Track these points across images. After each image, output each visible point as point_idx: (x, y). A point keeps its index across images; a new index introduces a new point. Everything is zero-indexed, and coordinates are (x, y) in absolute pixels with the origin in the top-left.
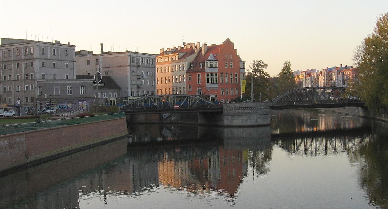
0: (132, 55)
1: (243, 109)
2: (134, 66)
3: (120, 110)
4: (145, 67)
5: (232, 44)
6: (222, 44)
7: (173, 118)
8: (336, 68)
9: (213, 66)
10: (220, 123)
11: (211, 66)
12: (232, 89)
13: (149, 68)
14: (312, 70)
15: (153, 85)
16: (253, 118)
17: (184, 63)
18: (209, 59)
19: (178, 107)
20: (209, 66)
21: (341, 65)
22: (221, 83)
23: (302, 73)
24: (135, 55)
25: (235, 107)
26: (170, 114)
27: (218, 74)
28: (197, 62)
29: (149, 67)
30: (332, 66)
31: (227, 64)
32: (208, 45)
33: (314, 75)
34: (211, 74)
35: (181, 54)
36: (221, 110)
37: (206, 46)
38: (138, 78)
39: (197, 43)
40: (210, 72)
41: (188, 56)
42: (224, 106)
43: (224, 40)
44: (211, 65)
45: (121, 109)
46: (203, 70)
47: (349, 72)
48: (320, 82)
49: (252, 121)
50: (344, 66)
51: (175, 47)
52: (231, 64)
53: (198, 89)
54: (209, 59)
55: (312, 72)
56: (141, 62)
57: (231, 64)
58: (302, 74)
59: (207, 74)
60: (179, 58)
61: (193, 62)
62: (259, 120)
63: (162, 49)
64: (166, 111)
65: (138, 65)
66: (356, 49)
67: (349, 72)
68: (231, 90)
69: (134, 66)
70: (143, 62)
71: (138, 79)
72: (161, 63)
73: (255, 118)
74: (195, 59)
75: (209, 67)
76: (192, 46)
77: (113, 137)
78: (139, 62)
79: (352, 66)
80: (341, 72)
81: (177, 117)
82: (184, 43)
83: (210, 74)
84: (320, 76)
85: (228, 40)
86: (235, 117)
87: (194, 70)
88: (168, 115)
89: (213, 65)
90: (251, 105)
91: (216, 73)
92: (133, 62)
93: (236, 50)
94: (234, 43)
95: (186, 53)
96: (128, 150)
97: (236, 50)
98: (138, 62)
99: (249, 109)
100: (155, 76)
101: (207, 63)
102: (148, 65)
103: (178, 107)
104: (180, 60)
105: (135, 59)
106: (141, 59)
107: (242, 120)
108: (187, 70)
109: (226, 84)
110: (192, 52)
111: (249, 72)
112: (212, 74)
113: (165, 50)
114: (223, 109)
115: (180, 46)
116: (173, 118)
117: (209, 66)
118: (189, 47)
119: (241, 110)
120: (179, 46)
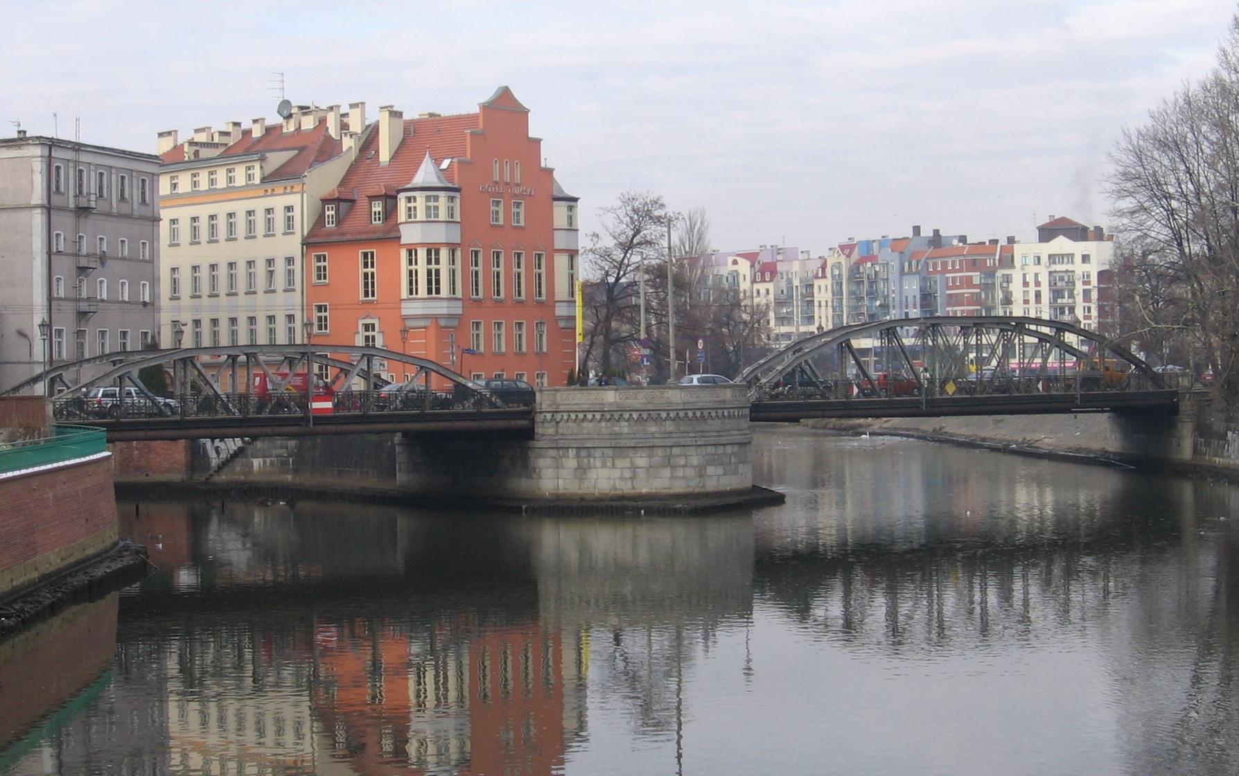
0: (53, 155)
1: (635, 415)
2: (64, 209)
3: (52, 421)
4: (109, 214)
5: (521, 114)
6: (477, 110)
7: (257, 463)
8: (898, 244)
9: (437, 215)
10: (522, 485)
11: (428, 215)
12: (520, 325)
13: (131, 221)
14: (779, 251)
15: (145, 304)
16: (682, 462)
17: (294, 200)
18: (419, 179)
19: (329, 405)
20: (421, 215)
21: (917, 230)
22: (538, 298)
23: (735, 262)
24: (69, 155)
25: (598, 408)
26: (243, 441)
27: (458, 253)
28: (356, 197)
29: (127, 217)
30: (873, 233)
31: (501, 208)
32: (406, 117)
33: (794, 270)
34: (429, 252)
35: (277, 159)
36: (524, 423)
37: (396, 121)
38: (79, 268)
39: (352, 106)
40: (422, 245)
41: (311, 166)
42: (543, 401)
43: (487, 96)
44: (428, 208)
45: (58, 413)
46: (390, 236)
47: (953, 263)
48: (820, 302)
49: (680, 472)
50: (927, 232)
51: (236, 124)
52: (496, 208)
53: (361, 322)
54: (419, 179)
55: (780, 257)
56: (93, 191)
57: (496, 208)
58: (735, 268)
59: (410, 255)
60: (266, 175)
61: (337, 195)
62: (710, 470)
63: (169, 133)
64: (220, 428)
65: (83, 203)
66: (1124, 144)
67: (953, 263)
68: (516, 332)
69: (64, 209)
70: (101, 188)
71: (82, 270)
72: (175, 198)
73: (695, 460)
74: (343, 183)
75: (418, 219)
76: (322, 121)
77: (78, 556)
78: (85, 192)
79: (965, 237)
80: (914, 262)
81: (278, 456)
82: (285, 109)
83: (422, 254)
84: (817, 277)
85: (505, 95)
86: (598, 453)
87: (344, 234)
88: (233, 445)
89: (436, 208)
90: (639, 399)
91: (453, 248)
92: (58, 187)
93: (538, 142)
94: (529, 111)
95: (297, 152)
96: (119, 621)
97: (538, 142)
98: (81, 192)
99: (664, 415)
100: (155, 260)
101: (409, 199)
102: (125, 209)
103: (329, 405)
104: (292, 184)
105: (67, 178)
106: (93, 174)
107: (634, 468)
108: (305, 233)
109: (492, 299)
110: (327, 149)
111: (597, 246)
112: (433, 252)
113: (182, 138)
114: (539, 418)
115: (25, 132)
116: (261, 460)
117: (421, 215)
118: (308, 123)
119: (628, 420)
120: (255, 121)
